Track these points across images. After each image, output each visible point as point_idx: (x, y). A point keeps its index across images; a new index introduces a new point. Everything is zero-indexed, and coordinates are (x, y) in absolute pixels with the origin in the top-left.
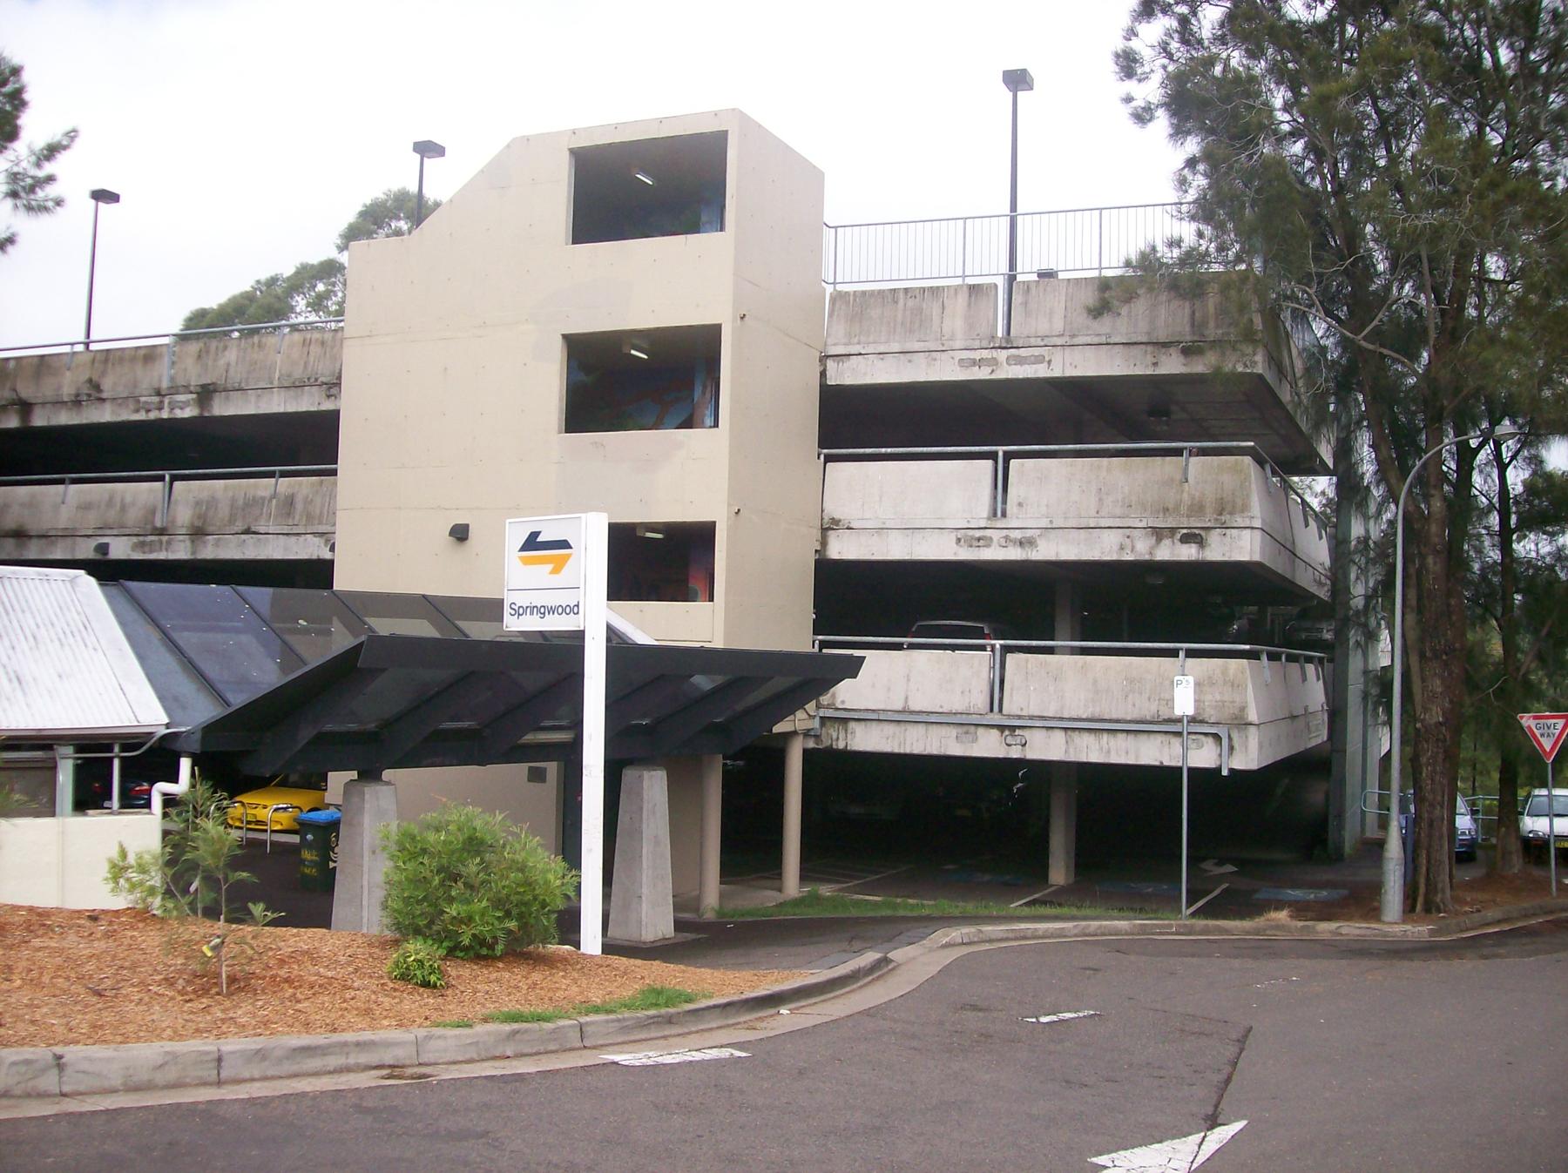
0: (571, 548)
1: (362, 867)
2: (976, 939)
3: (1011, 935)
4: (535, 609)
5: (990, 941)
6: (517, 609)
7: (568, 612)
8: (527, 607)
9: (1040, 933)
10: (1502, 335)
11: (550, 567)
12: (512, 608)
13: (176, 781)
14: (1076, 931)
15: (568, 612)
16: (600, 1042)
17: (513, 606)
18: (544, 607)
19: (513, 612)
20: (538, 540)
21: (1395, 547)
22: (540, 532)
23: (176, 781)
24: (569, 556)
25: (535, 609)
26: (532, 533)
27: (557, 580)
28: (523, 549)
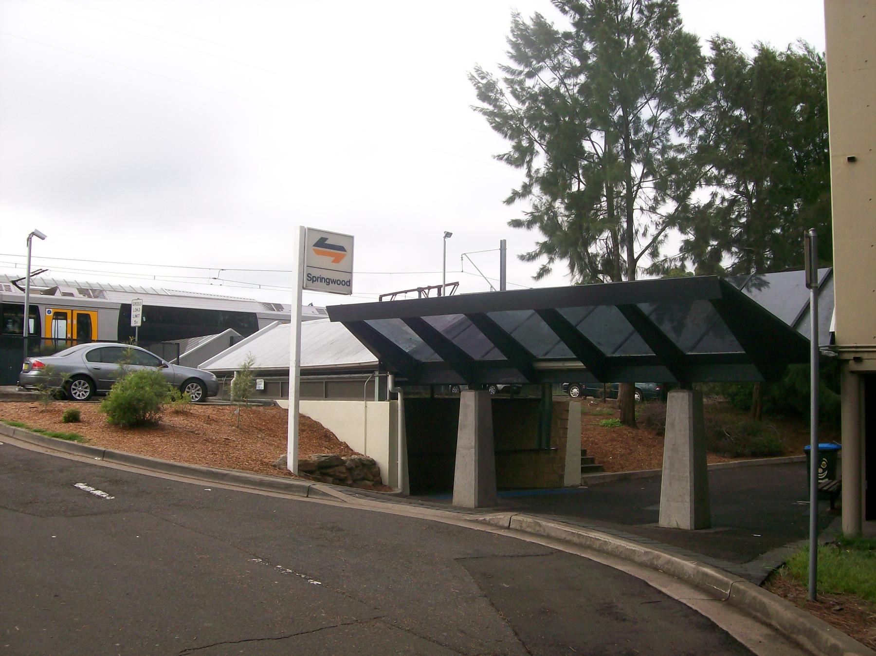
0: (345, 251)
1: (72, 346)
2: (529, 530)
3: (575, 539)
4: (323, 280)
5: (548, 537)
6: (312, 277)
7: (343, 282)
8: (318, 277)
9: (610, 548)
10: (595, 59)
11: (332, 259)
12: (309, 277)
13: (78, 314)
14: (644, 558)
15: (343, 282)
16: (18, 438)
17: (309, 275)
18: (329, 279)
19: (310, 279)
20: (326, 242)
21: (833, 292)
22: (327, 239)
23: (78, 314)
24: (344, 255)
25: (323, 280)
26: (343, 247)
27: (334, 266)
28: (316, 245)
